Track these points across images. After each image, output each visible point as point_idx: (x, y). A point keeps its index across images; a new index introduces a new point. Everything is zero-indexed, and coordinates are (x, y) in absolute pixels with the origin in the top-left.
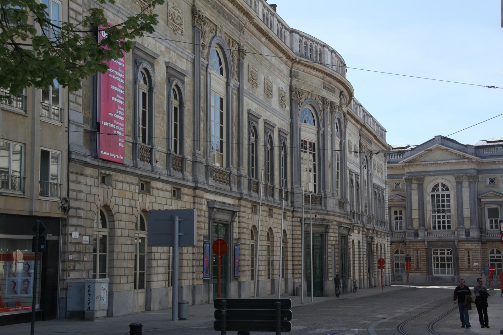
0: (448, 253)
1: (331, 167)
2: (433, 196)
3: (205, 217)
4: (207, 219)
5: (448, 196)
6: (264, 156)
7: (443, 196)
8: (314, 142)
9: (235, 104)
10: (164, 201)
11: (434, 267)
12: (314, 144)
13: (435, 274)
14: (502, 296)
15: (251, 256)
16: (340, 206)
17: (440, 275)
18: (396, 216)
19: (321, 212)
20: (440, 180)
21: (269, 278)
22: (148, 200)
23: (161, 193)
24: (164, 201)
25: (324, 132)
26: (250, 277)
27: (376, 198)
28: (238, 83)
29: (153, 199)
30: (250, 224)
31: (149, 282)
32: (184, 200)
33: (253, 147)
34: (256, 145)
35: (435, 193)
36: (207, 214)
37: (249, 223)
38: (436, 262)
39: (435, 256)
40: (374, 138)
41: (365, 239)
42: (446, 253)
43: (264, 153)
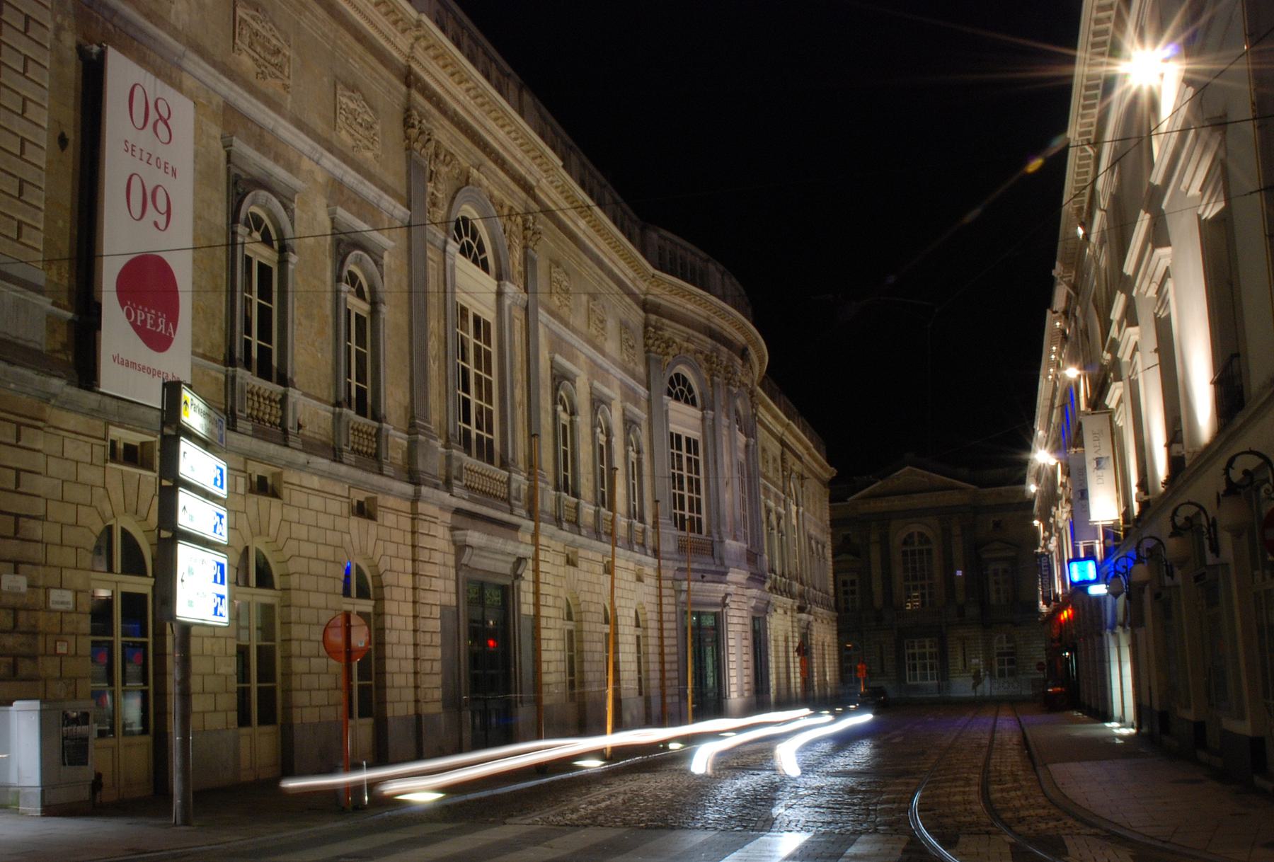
0: (931, 647)
1: (730, 486)
2: (905, 553)
3: (445, 565)
4: (453, 572)
5: (929, 552)
6: (591, 453)
7: (921, 552)
8: (696, 438)
9: (519, 337)
10: (325, 521)
11: (909, 670)
12: (696, 442)
13: (910, 680)
14: (278, 562)
15: (635, 655)
16: (748, 560)
17: (919, 682)
18: (845, 589)
19: (713, 568)
20: (916, 528)
21: (640, 694)
22: (276, 515)
23: (317, 502)
24: (325, 521)
25: (713, 420)
26: (233, 716)
27: (811, 556)
28: (525, 296)
29: (293, 514)
30: (562, 587)
31: (288, 707)
32: (386, 523)
33: (565, 435)
34: (572, 431)
35: (908, 548)
36: (451, 560)
37: (559, 584)
38: (911, 662)
39: (911, 651)
40: (805, 452)
41: (795, 624)
42: (927, 647)
43: (591, 447)
